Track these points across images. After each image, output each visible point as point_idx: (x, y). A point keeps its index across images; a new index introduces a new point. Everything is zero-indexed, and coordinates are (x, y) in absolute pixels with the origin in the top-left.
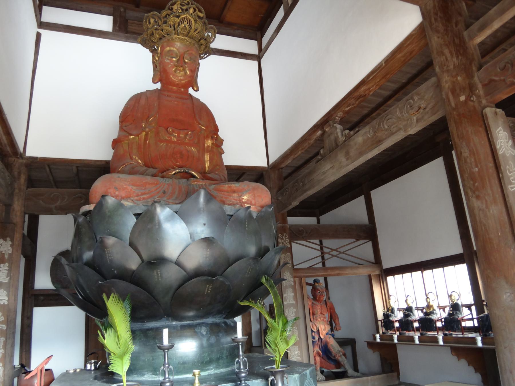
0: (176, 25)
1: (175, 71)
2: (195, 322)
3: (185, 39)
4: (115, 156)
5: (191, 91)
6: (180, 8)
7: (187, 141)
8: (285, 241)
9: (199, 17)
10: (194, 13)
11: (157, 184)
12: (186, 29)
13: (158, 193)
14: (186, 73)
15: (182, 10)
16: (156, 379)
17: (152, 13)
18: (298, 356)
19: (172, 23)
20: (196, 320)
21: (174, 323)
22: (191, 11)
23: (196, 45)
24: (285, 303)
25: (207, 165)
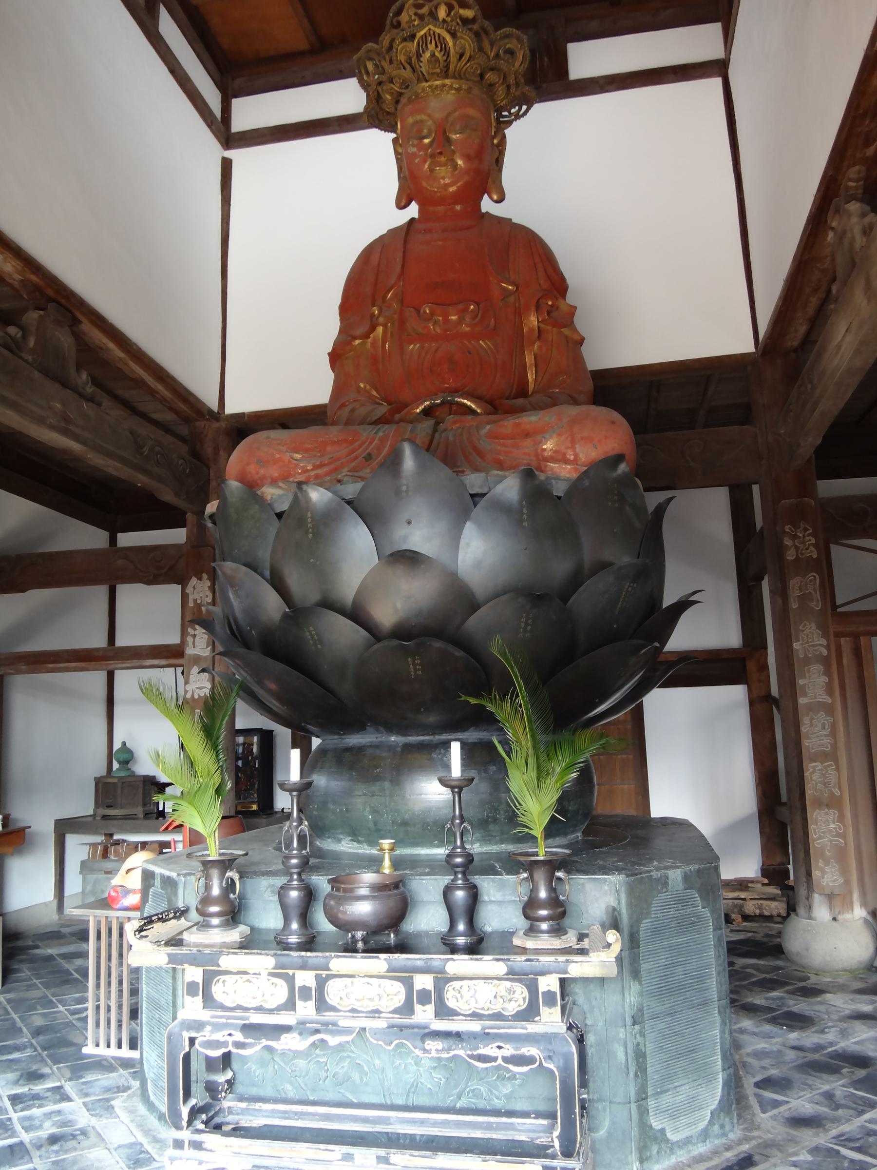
0: (414, 59)
1: (432, 170)
2: (437, 737)
3: (444, 85)
4: (338, 390)
5: (487, 205)
6: (416, 14)
7: (465, 328)
8: (803, 543)
9: (465, 21)
10: (448, 15)
11: (353, 441)
12: (437, 60)
13: (353, 460)
14: (455, 167)
15: (421, 17)
16: (361, 851)
17: (364, 48)
18: (838, 835)
19: (402, 58)
20: (440, 734)
21: (393, 739)
22: (442, 13)
23: (476, 91)
24: (802, 701)
25: (531, 377)
